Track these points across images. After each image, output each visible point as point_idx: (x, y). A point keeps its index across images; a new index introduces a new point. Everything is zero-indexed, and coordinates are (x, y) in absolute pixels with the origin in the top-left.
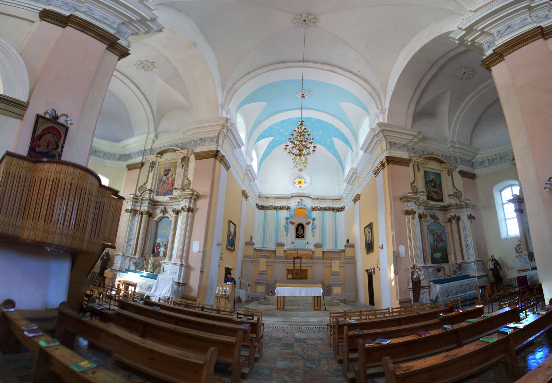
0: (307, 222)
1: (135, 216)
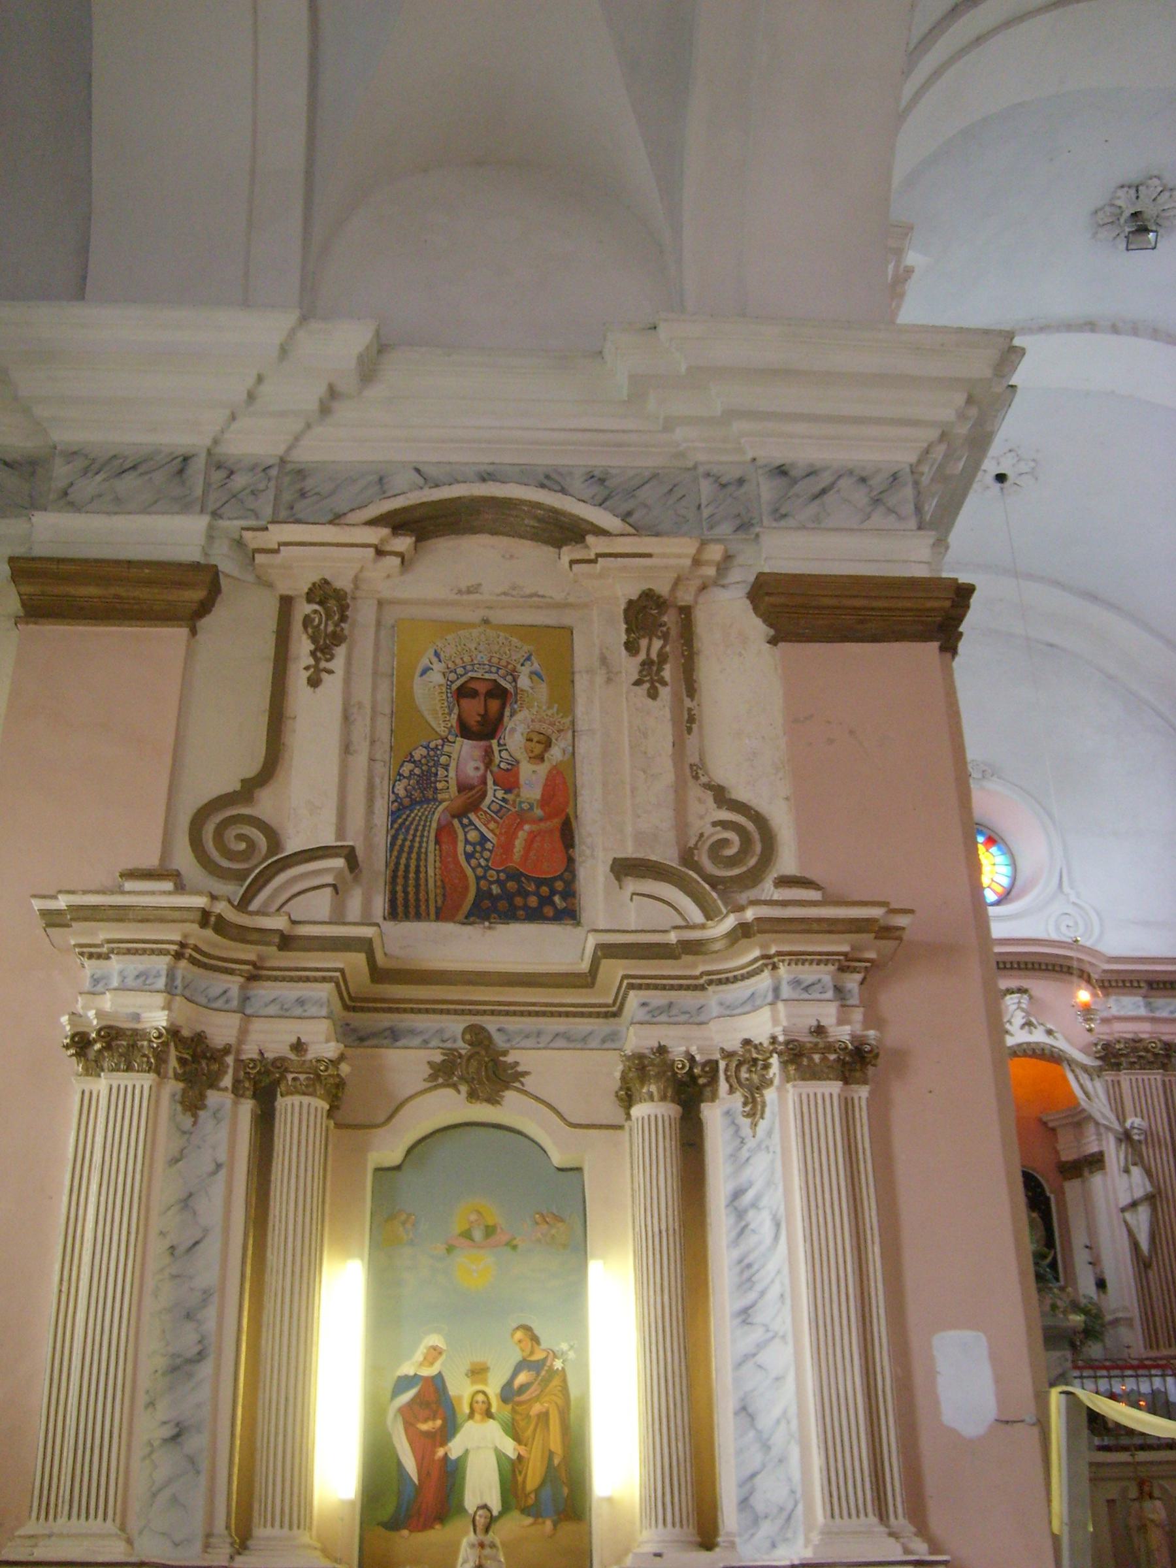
1: (192, 1104)
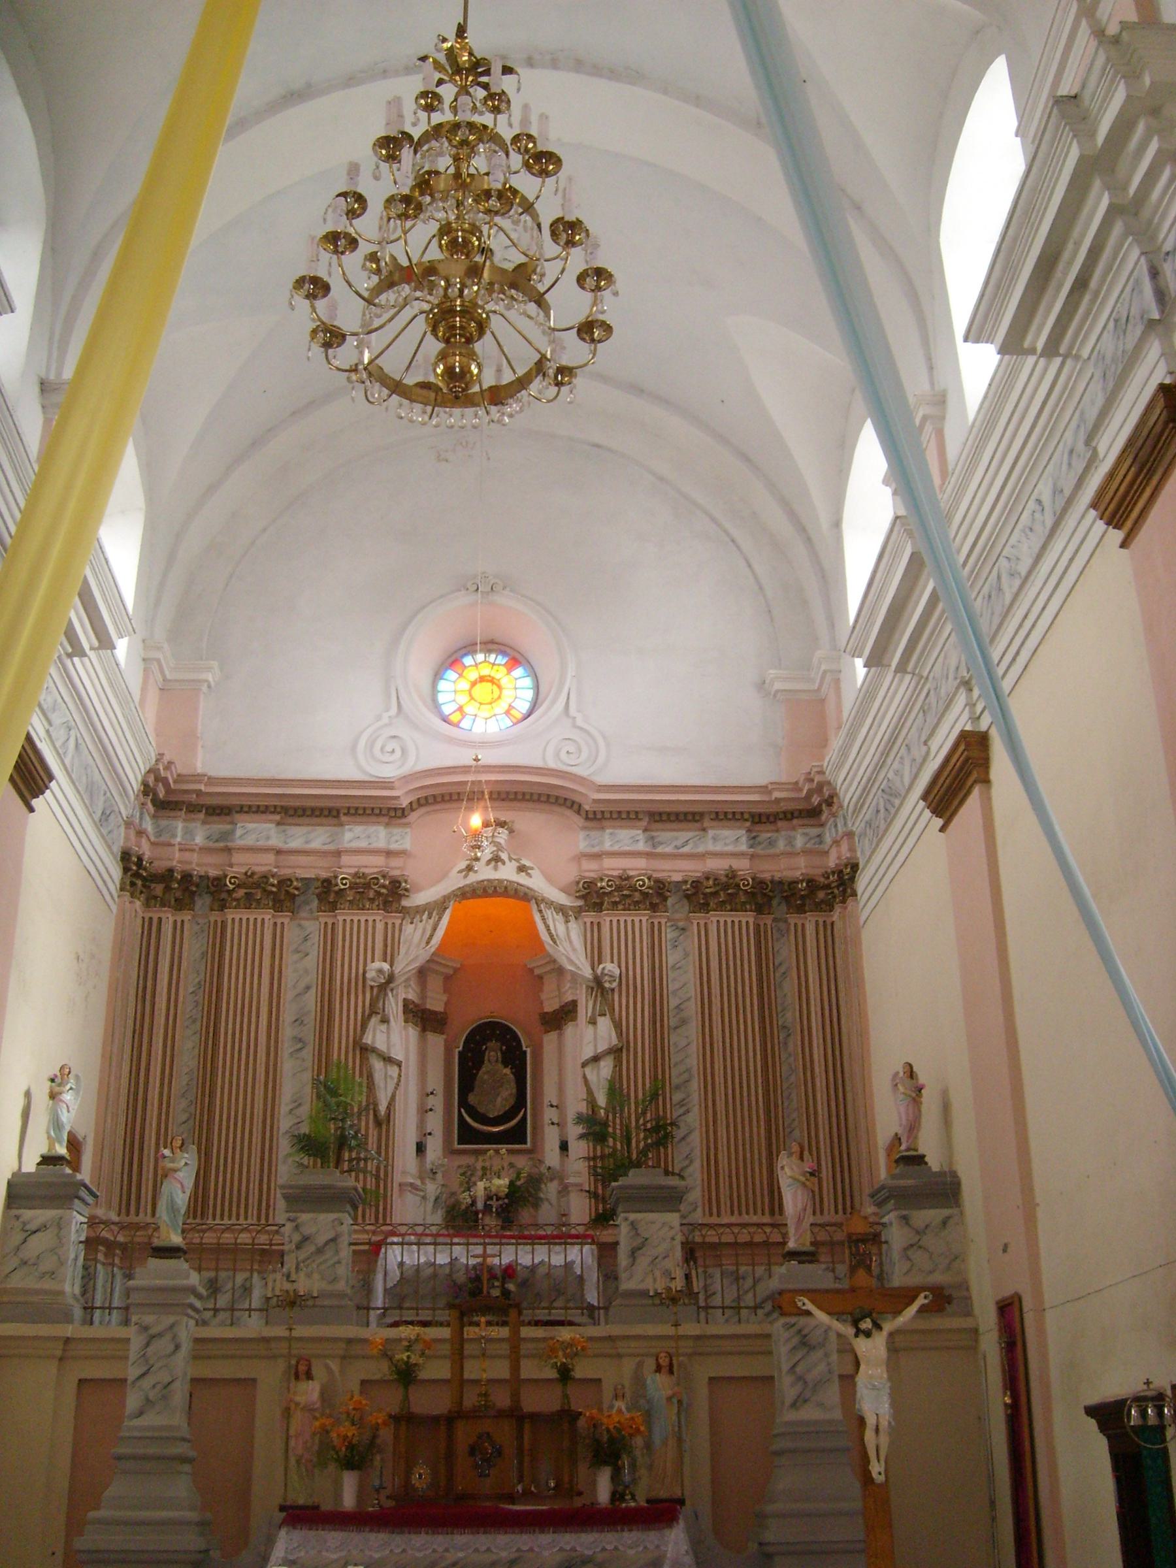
0: (550, 1006)
